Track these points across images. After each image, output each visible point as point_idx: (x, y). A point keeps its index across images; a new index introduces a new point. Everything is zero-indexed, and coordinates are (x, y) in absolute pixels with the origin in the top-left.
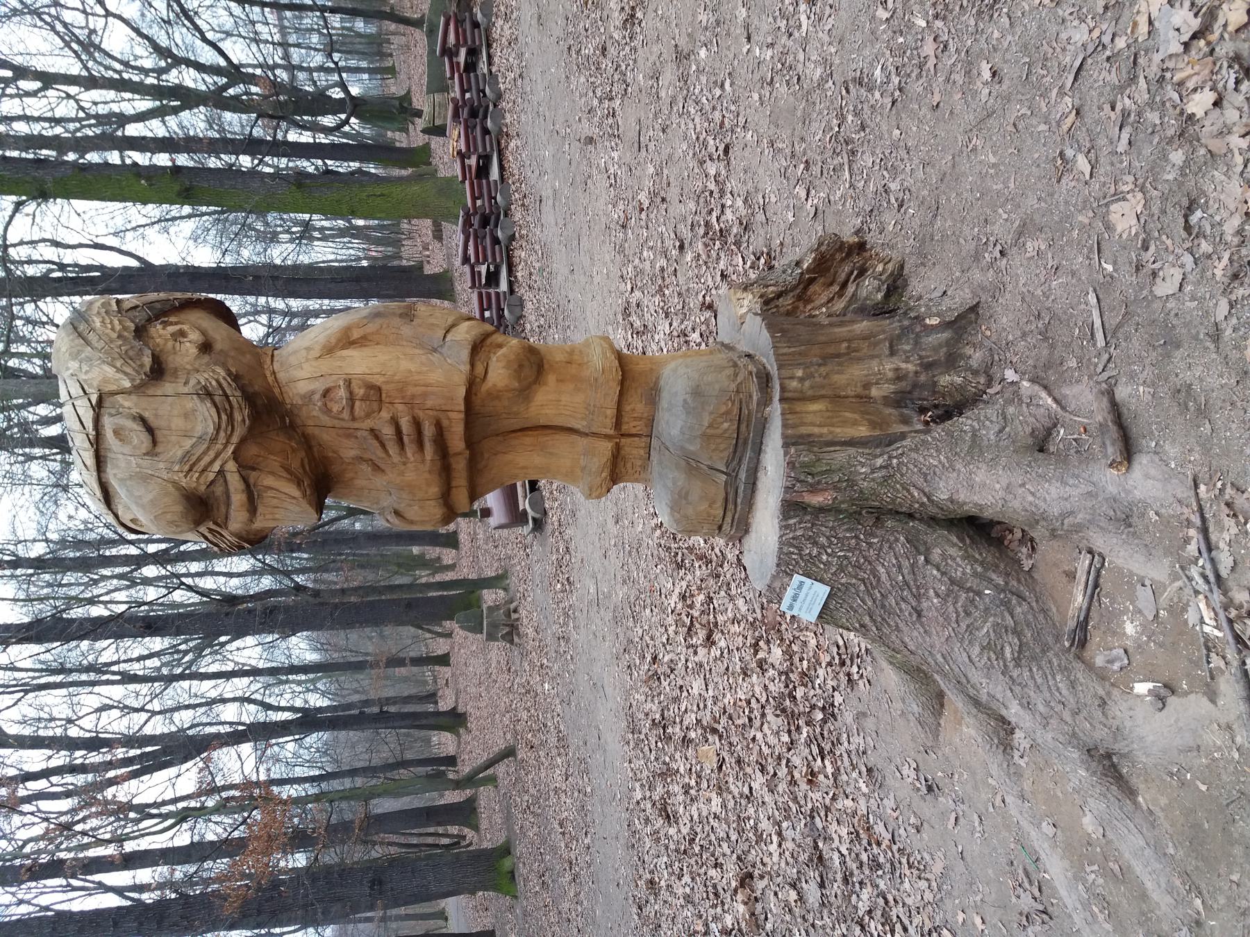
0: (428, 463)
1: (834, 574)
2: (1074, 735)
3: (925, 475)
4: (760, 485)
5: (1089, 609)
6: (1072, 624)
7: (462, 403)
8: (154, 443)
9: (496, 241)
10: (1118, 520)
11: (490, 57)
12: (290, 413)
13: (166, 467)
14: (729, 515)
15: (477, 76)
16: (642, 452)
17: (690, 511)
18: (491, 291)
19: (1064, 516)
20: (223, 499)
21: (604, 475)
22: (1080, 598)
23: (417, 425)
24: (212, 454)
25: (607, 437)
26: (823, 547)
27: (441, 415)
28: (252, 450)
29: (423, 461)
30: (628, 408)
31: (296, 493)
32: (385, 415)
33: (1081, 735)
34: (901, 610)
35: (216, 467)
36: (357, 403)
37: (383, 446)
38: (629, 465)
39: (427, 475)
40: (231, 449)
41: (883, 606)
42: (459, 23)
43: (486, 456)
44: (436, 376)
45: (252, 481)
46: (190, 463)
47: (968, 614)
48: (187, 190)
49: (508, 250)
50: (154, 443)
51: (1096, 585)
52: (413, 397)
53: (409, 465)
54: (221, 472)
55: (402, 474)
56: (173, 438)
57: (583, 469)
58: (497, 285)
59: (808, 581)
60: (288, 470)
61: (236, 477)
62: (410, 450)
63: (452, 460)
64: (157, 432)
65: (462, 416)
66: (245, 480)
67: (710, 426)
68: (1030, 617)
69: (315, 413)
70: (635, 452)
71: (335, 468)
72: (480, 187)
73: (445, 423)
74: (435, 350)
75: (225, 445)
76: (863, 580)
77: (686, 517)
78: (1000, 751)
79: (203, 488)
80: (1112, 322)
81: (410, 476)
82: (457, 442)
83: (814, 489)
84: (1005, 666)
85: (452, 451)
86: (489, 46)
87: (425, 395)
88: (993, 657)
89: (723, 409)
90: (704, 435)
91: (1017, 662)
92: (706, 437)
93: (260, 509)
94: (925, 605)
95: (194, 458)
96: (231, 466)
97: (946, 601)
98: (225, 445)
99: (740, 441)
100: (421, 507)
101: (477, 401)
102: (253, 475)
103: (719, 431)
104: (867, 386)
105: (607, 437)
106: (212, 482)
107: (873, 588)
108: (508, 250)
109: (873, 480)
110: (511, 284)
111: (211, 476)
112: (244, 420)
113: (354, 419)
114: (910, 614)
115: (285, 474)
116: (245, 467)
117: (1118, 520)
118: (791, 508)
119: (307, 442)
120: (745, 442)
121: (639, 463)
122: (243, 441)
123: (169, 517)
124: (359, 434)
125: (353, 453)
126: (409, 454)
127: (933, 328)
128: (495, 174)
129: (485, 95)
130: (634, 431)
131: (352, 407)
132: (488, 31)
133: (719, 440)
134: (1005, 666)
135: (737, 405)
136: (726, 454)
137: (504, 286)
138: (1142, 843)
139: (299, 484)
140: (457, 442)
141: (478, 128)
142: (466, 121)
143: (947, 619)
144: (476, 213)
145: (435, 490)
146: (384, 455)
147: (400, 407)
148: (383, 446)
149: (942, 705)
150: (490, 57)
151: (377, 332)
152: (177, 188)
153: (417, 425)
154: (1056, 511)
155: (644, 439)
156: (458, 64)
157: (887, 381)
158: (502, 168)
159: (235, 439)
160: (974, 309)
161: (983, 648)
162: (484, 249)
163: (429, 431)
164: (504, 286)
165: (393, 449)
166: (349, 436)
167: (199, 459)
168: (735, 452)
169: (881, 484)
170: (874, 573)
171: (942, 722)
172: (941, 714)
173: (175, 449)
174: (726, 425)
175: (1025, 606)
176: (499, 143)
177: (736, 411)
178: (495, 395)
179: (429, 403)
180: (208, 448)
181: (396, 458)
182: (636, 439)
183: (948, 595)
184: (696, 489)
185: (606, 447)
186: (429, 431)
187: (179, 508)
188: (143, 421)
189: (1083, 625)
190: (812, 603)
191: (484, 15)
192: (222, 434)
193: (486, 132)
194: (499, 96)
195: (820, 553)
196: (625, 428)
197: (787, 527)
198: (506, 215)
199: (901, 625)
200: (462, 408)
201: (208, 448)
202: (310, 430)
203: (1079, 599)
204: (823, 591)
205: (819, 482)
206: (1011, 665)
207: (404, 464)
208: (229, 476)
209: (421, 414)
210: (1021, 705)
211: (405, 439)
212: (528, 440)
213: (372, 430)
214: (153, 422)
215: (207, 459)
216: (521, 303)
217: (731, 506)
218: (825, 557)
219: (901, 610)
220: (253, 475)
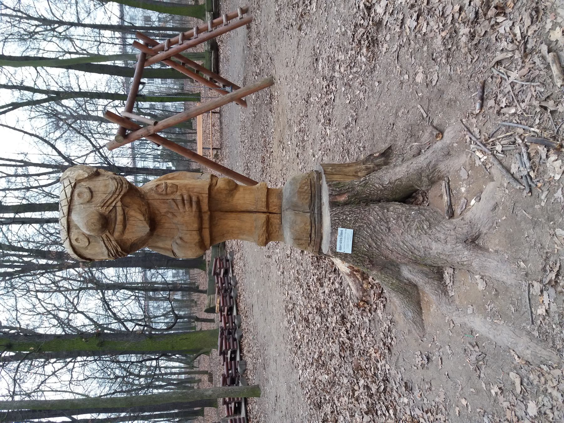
0: (194, 213)
1: (353, 224)
2: (457, 238)
3: (379, 178)
4: (323, 214)
5: (450, 200)
6: (446, 208)
7: (207, 190)
8: (92, 197)
9: (235, 340)
10: (446, 155)
11: (233, 271)
12: (143, 195)
13: (95, 208)
14: (313, 229)
15: (232, 317)
16: (278, 221)
17: (297, 228)
18: (237, 417)
19: (428, 165)
20: (114, 219)
21: (264, 228)
22: (446, 198)
23: (190, 198)
24: (113, 199)
25: (263, 212)
26: (348, 215)
27: (200, 195)
28: (127, 200)
29: (192, 211)
30: (271, 201)
31: (142, 218)
32: (178, 193)
33: (459, 236)
34: (382, 230)
35: (113, 204)
36: (168, 188)
37: (177, 205)
38: (274, 227)
39: (193, 218)
40: (120, 197)
41: (375, 231)
42: (221, 260)
43: (217, 219)
44: (198, 183)
45: (126, 212)
46: (104, 204)
47: (407, 222)
48: (102, 342)
49: (240, 342)
50: (92, 197)
51: (449, 189)
52: (189, 188)
53: (187, 213)
54: (115, 207)
55: (183, 217)
56: (100, 195)
57: (255, 227)
58: (240, 413)
59: (344, 229)
60: (140, 211)
61: (120, 208)
62: (187, 207)
63: (203, 215)
64: (94, 193)
65: (207, 195)
66: (123, 210)
67: (300, 188)
68: (431, 215)
69: (153, 194)
70: (275, 221)
71: (158, 218)
72: (228, 318)
73: (201, 198)
74: (198, 178)
75: (118, 195)
76: (365, 223)
77: (296, 230)
78: (443, 295)
79: (107, 213)
80: (426, 107)
81: (187, 218)
82: (205, 207)
83: (340, 194)
84: (426, 232)
85: (203, 211)
86: (232, 267)
87: (194, 188)
88: (420, 230)
89: (304, 182)
90: (298, 192)
91: (430, 228)
92: (300, 193)
93: (128, 227)
94: (390, 225)
95: (105, 201)
96: (119, 204)
97: (398, 220)
98: (118, 195)
99: (313, 195)
100: (191, 235)
101: (213, 193)
102: (127, 209)
103: (304, 190)
104: (356, 172)
105: (263, 212)
106: (111, 211)
107: (370, 225)
108: (240, 342)
109: (361, 186)
110: (241, 357)
111: (111, 208)
112: (126, 187)
113: (167, 194)
114: (386, 230)
115: (139, 211)
116: (124, 206)
117: (446, 155)
118: (333, 204)
119: (148, 205)
120: (315, 196)
121: (278, 226)
122: (124, 195)
123: (92, 220)
124: (168, 201)
125: (165, 210)
126: (187, 208)
127: (377, 157)
128: (235, 313)
129: (231, 284)
130: (274, 211)
131: (167, 189)
132: (232, 261)
133: (304, 194)
134: (426, 232)
135: (309, 180)
136: (308, 201)
137: (243, 414)
138: (496, 263)
139: (144, 215)
140: (205, 207)
141: (231, 339)
142: (223, 294)
143: (400, 226)
144: (228, 376)
145: (196, 226)
146: (177, 209)
147: (184, 191)
148: (177, 205)
149: (421, 309)
150: (233, 271)
151: (178, 176)
152: (97, 342)
153: (190, 198)
154: (425, 165)
155: (278, 215)
156: (227, 358)
157: (363, 170)
158: (237, 310)
159: (122, 193)
160: (390, 148)
161: (416, 230)
162: (229, 344)
163: (194, 199)
164: (243, 414)
165: (180, 206)
166: (164, 203)
167: (107, 202)
168: (311, 202)
169: (364, 187)
170: (368, 219)
171: (424, 318)
172: (421, 313)
173: (99, 198)
174: (306, 187)
175: (428, 212)
176: (236, 301)
177: (309, 182)
178: (220, 191)
179: (195, 190)
180: (112, 197)
181: (181, 210)
182: (276, 215)
183: (398, 218)
184: (299, 219)
185: (263, 217)
186: (194, 199)
187: (97, 217)
188: (90, 189)
189: (450, 206)
190: (348, 245)
191: (230, 256)
192: (118, 191)
193: (231, 297)
194: (236, 283)
195: (346, 218)
196: (270, 209)
197: (332, 211)
198: (239, 328)
199: (384, 237)
200: (207, 192)
201: (112, 197)
202: (150, 201)
203: (446, 198)
204: (350, 232)
205: (341, 190)
206: (428, 230)
207: (185, 212)
208: (117, 208)
209: (192, 194)
210: (436, 242)
211: (185, 201)
212: (233, 215)
213: (173, 199)
214: (93, 189)
215: (111, 201)
216: (246, 363)
217: (313, 225)
218: (349, 218)
219: (382, 230)
220: (127, 209)
